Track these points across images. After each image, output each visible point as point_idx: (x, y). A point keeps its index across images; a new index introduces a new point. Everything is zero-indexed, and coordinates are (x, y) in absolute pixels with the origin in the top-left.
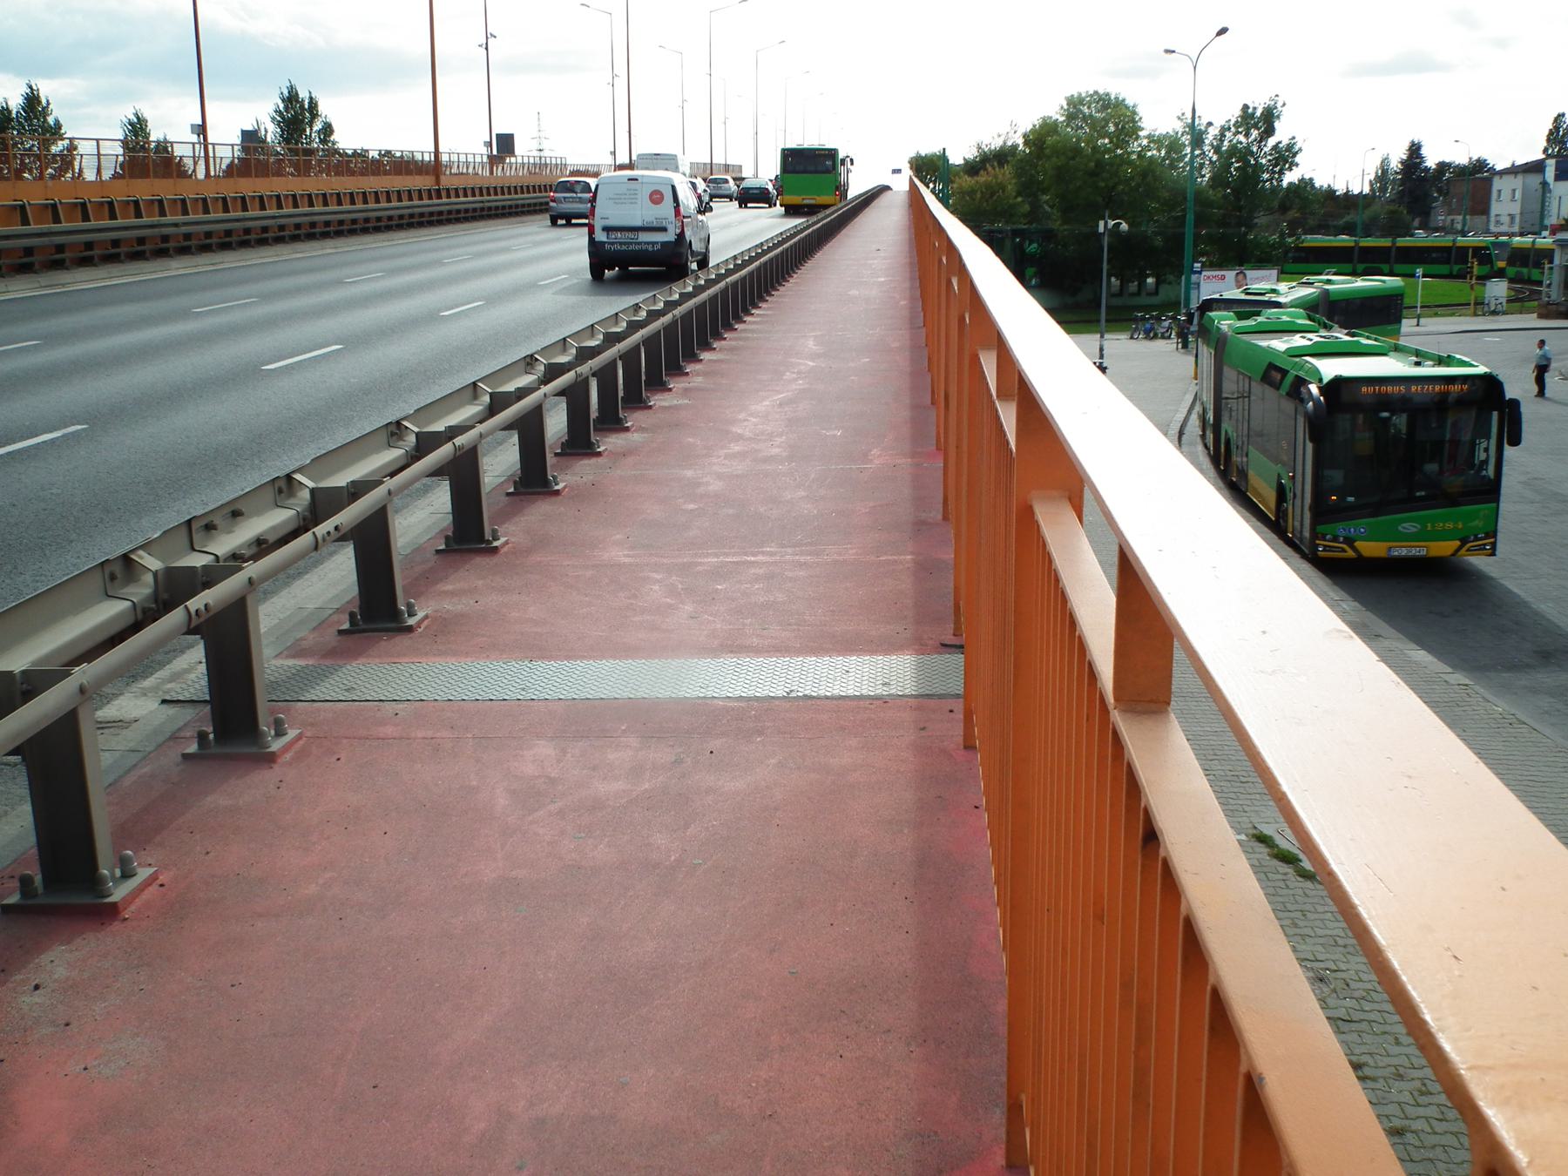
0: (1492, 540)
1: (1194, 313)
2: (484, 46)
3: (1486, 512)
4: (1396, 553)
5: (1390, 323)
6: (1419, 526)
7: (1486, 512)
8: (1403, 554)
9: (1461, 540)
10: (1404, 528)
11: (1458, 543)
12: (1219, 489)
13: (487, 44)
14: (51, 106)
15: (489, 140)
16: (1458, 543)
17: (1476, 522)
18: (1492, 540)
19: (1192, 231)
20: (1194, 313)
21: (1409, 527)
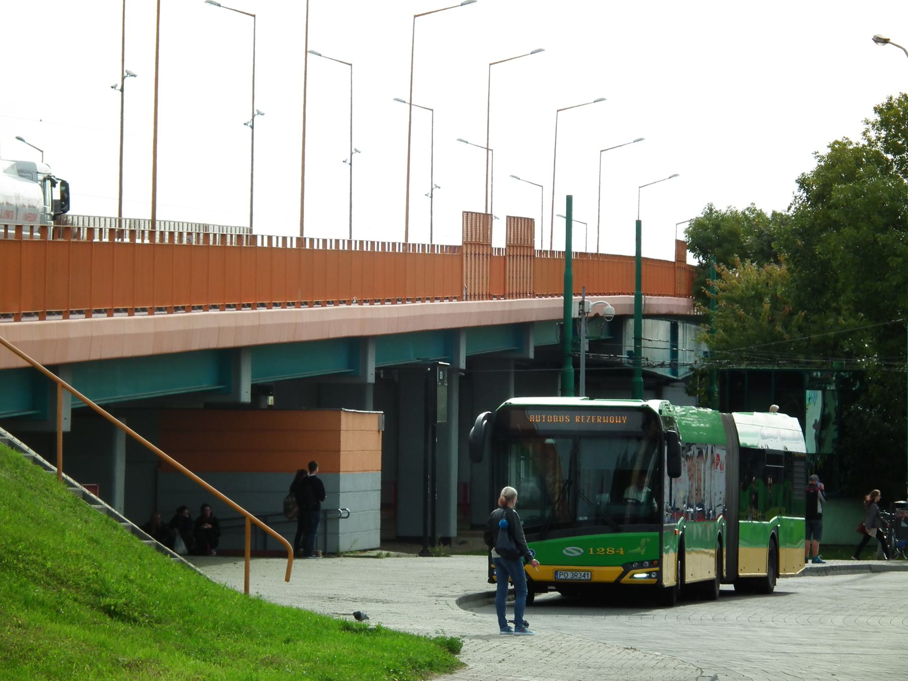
0: (657, 569)
1: (819, 554)
2: (430, 195)
3: (648, 540)
4: (562, 577)
5: (468, 356)
6: (582, 551)
7: (648, 540)
8: (569, 577)
9: (623, 566)
10: (567, 551)
11: (621, 569)
12: (26, 181)
13: (432, 194)
14: (840, 140)
15: (150, 218)
16: (621, 569)
17: (638, 550)
18: (657, 569)
19: (581, 369)
20: (819, 554)
21: (573, 551)
